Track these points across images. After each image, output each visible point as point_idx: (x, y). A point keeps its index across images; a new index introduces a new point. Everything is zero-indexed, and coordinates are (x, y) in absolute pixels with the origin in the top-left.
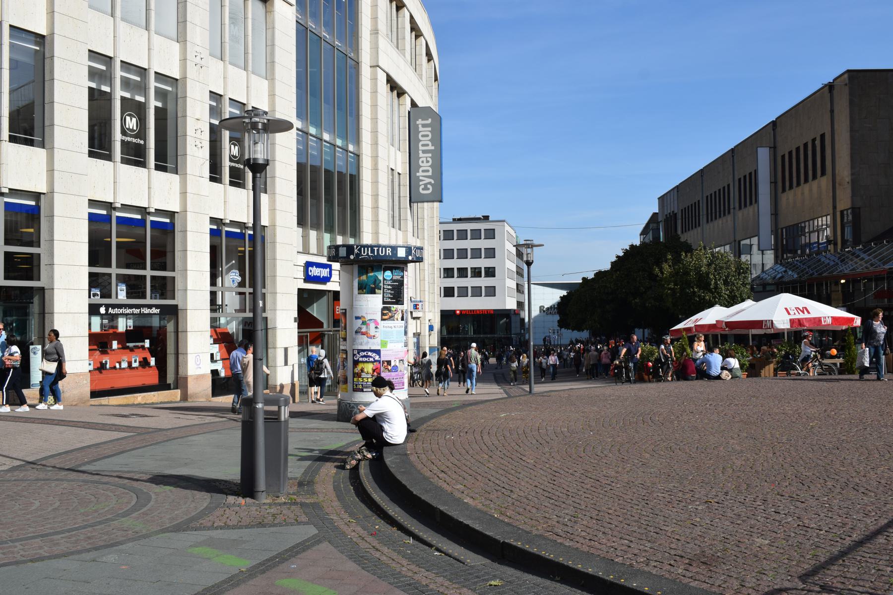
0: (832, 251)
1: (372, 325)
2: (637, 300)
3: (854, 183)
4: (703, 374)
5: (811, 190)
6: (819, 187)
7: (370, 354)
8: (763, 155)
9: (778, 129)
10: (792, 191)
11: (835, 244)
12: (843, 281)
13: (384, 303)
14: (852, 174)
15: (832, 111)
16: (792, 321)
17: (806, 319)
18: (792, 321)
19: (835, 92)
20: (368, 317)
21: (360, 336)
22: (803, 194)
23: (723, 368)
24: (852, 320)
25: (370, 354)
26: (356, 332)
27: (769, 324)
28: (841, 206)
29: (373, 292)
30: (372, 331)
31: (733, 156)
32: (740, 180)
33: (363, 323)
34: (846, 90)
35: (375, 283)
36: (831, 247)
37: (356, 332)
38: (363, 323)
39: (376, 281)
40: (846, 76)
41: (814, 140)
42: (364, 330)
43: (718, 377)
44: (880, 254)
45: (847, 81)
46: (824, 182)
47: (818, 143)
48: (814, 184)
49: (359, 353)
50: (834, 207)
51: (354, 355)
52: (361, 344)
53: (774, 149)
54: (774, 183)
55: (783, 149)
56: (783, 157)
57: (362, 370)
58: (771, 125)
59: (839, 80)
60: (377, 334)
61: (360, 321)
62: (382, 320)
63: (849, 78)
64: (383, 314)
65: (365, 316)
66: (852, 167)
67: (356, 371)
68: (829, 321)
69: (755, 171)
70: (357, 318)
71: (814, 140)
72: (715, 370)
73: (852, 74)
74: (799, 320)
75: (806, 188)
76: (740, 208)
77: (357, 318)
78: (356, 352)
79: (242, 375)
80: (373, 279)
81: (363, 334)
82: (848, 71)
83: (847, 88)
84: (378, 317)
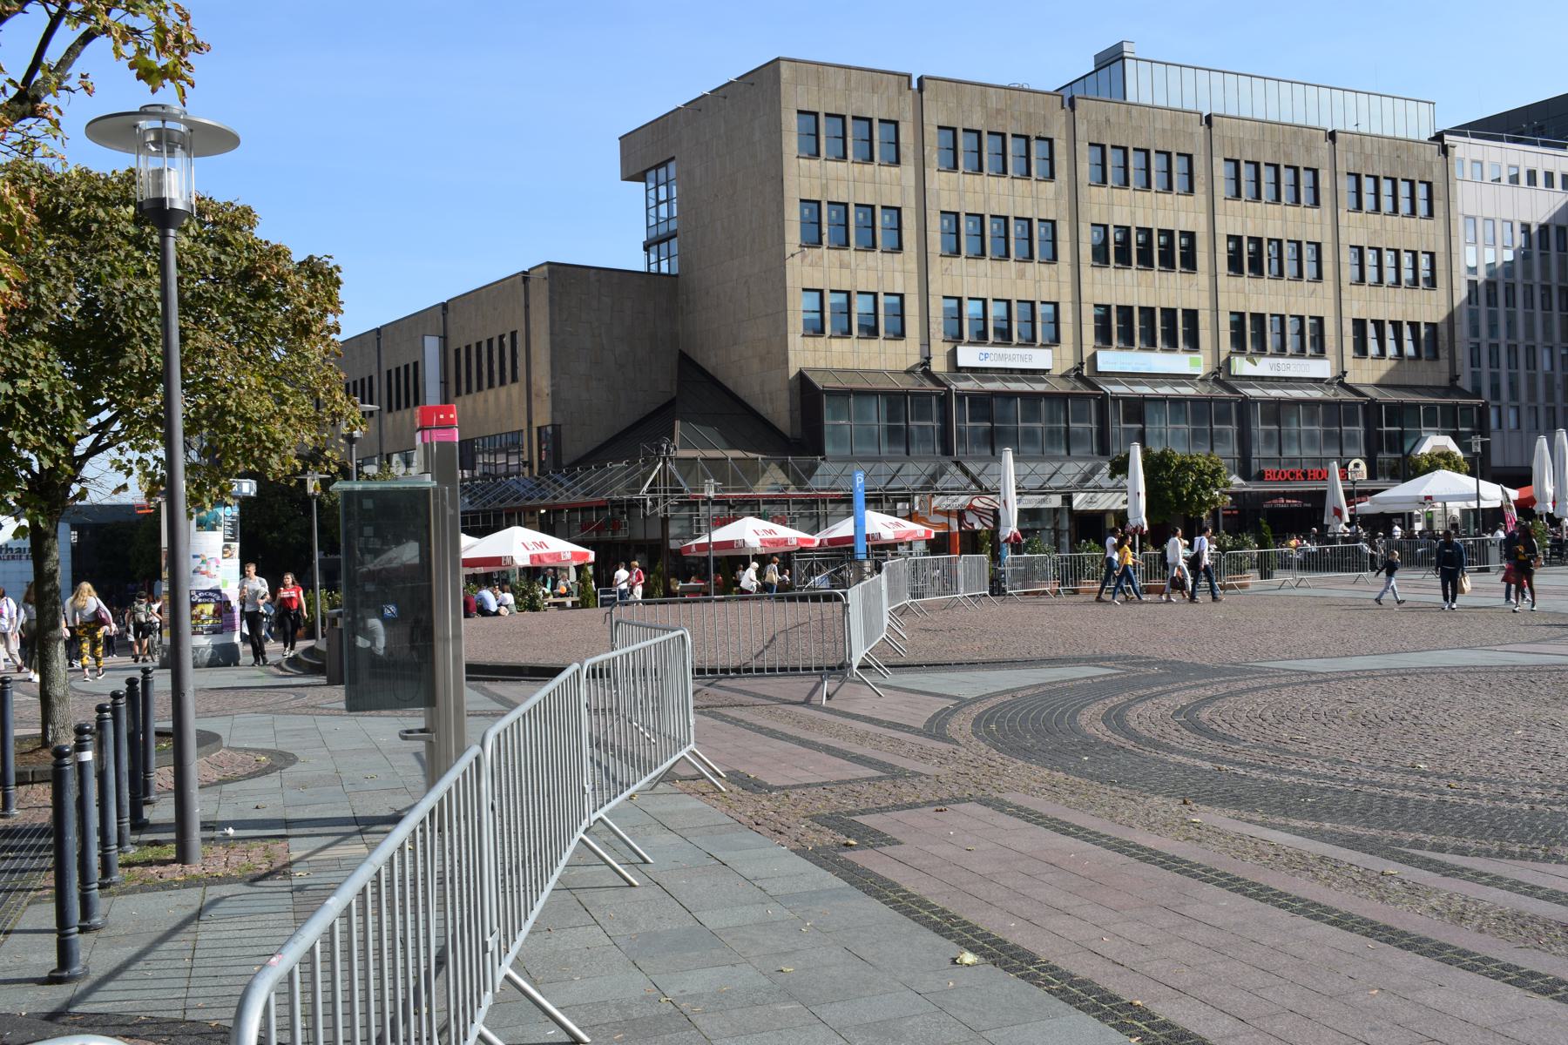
0: (527, 475)
1: (213, 564)
2: (275, 535)
3: (555, 396)
4: (484, 611)
5: (497, 398)
6: (509, 395)
7: (210, 594)
8: (432, 345)
9: (451, 315)
10: (471, 396)
11: (531, 467)
12: (543, 511)
13: (225, 540)
14: (552, 385)
15: (527, 307)
16: (532, 557)
17: (546, 554)
18: (532, 557)
19: (531, 284)
20: (208, 556)
21: (198, 576)
22: (486, 401)
23: (499, 605)
24: (586, 555)
25: (210, 594)
26: (194, 572)
27: (509, 561)
28: (537, 423)
29: (213, 528)
30: (213, 571)
31: (378, 339)
32: (389, 372)
33: (203, 562)
34: (546, 286)
35: (215, 520)
36: (526, 470)
37: (194, 572)
38: (203, 562)
39: (217, 518)
40: (545, 268)
41: (501, 337)
42: (204, 568)
43: (497, 614)
44: (588, 484)
45: (547, 275)
46: (516, 391)
47: (507, 340)
48: (503, 391)
49: (197, 594)
50: (530, 423)
51: (191, 596)
52: (200, 584)
53: (444, 339)
54: (445, 383)
55: (458, 341)
56: (457, 352)
57: (202, 612)
58: (441, 307)
59: (535, 271)
60: (218, 574)
61: (200, 560)
62: (224, 558)
63: (550, 272)
64: (224, 552)
65: (204, 553)
66: (553, 377)
67: (194, 612)
68: (795, 542)
69: (416, 364)
70: (195, 557)
71: (501, 337)
72: (493, 608)
73: (559, 274)
74: (539, 556)
75: (491, 394)
76: (390, 410)
77: (195, 557)
78: (194, 593)
79: (780, 556)
80: (214, 516)
81: (203, 573)
82: (549, 263)
83: (547, 282)
84: (219, 555)
